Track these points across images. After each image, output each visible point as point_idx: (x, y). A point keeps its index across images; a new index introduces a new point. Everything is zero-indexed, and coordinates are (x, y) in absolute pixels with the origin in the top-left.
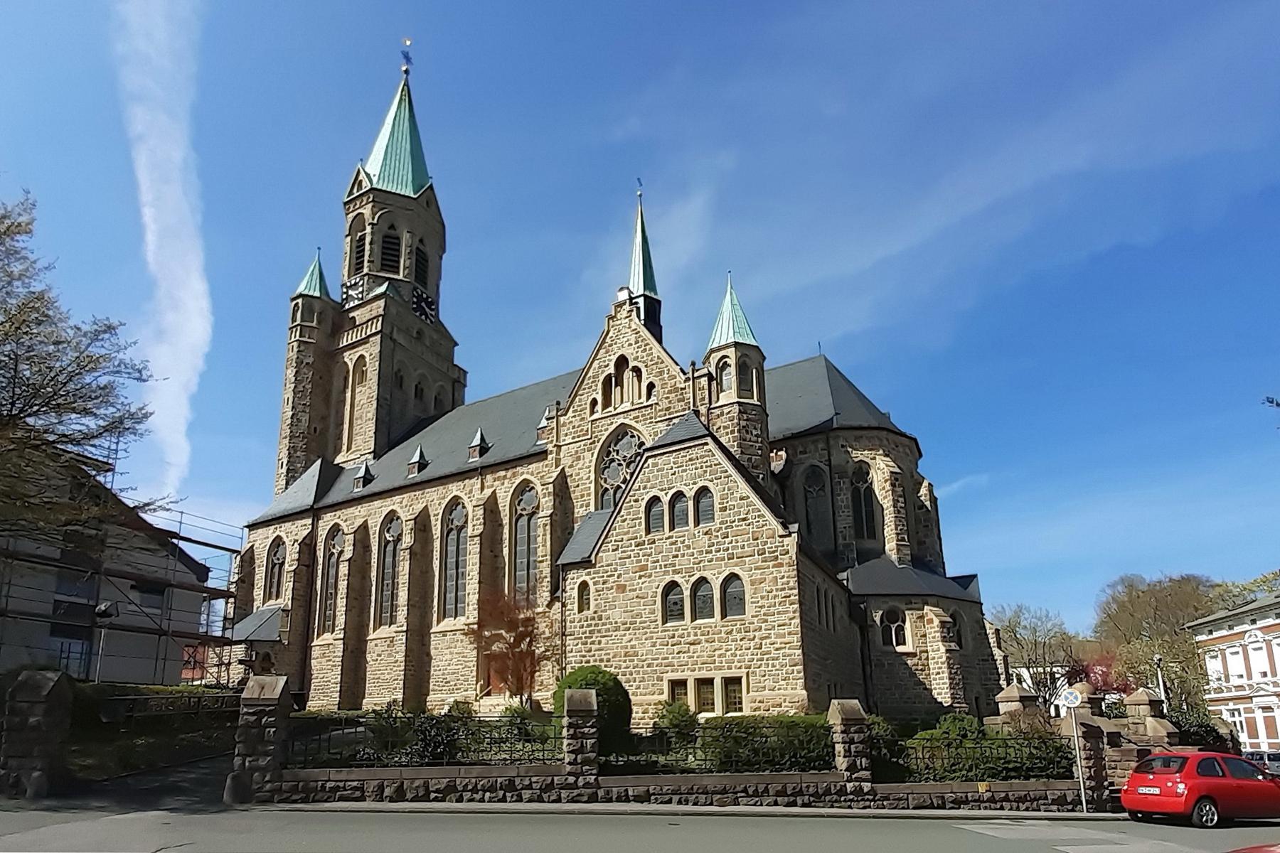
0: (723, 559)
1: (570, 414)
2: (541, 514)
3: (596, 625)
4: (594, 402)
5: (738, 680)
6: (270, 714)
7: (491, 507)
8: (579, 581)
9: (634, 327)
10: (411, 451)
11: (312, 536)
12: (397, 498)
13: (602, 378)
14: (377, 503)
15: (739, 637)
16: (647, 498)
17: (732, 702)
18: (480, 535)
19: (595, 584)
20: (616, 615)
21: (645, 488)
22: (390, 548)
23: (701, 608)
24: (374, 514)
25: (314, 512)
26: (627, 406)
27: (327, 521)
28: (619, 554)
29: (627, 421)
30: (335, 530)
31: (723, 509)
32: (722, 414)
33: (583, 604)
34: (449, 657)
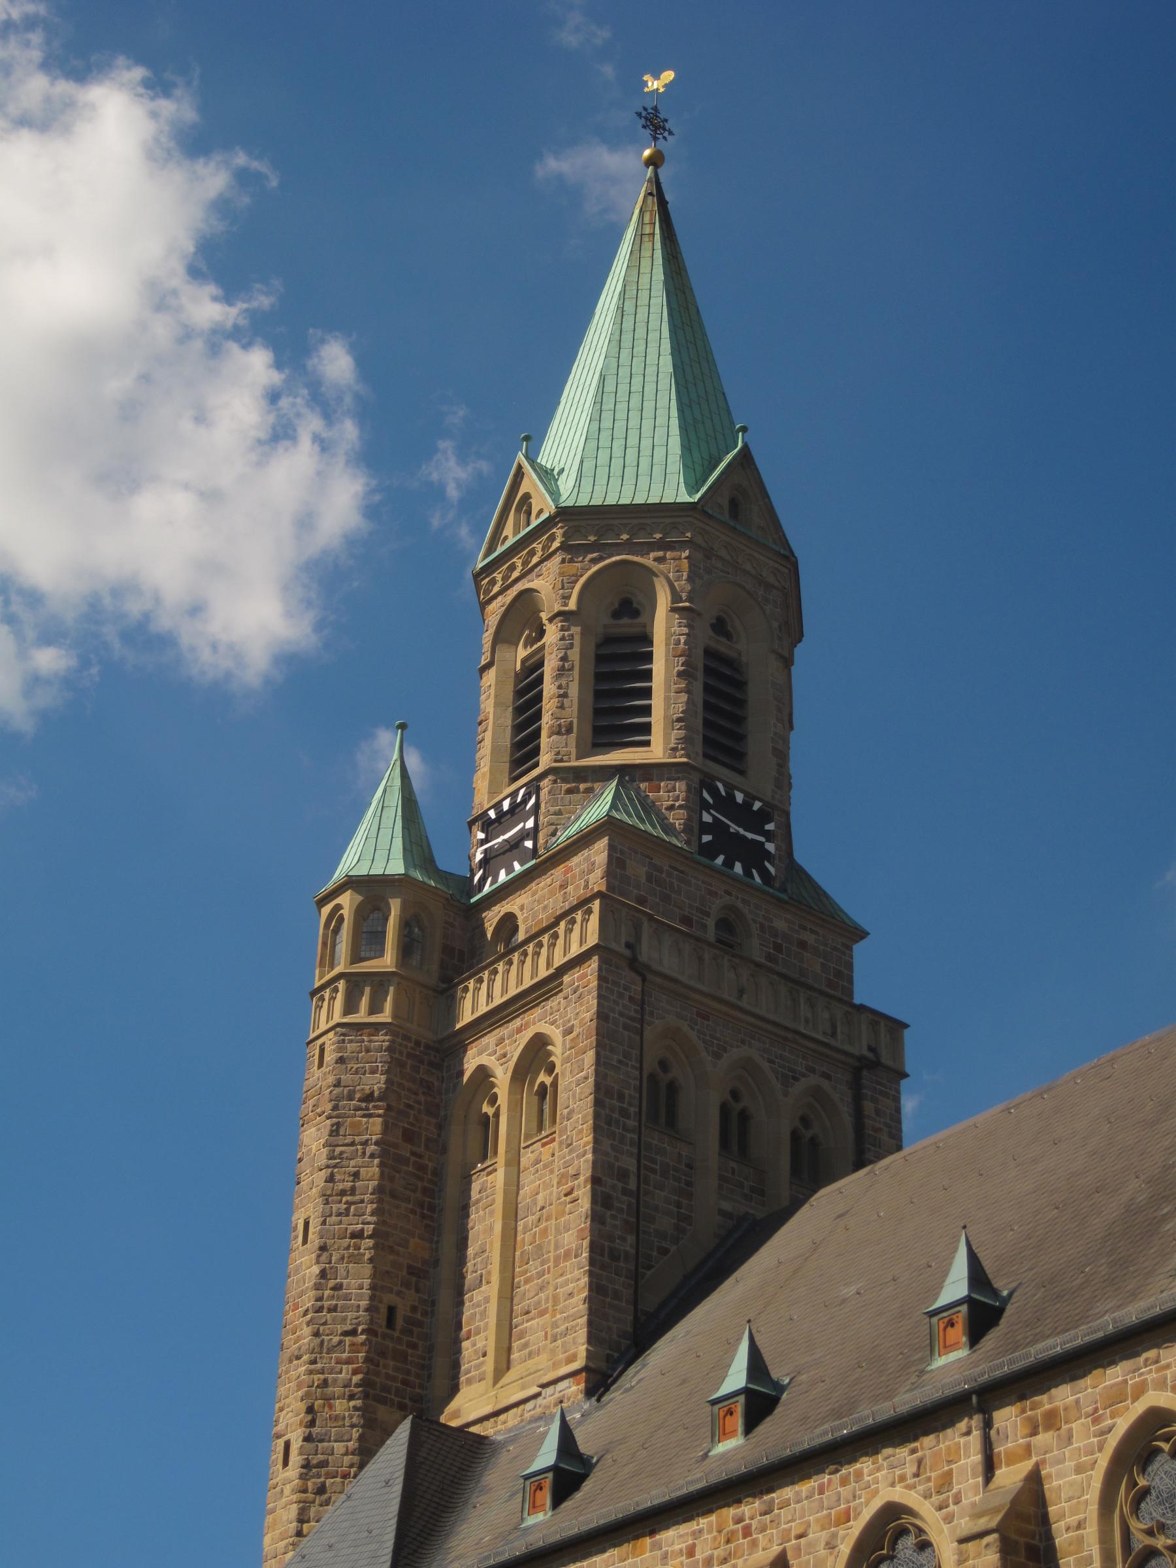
10: (709, 1348)
33: (546, 1333)
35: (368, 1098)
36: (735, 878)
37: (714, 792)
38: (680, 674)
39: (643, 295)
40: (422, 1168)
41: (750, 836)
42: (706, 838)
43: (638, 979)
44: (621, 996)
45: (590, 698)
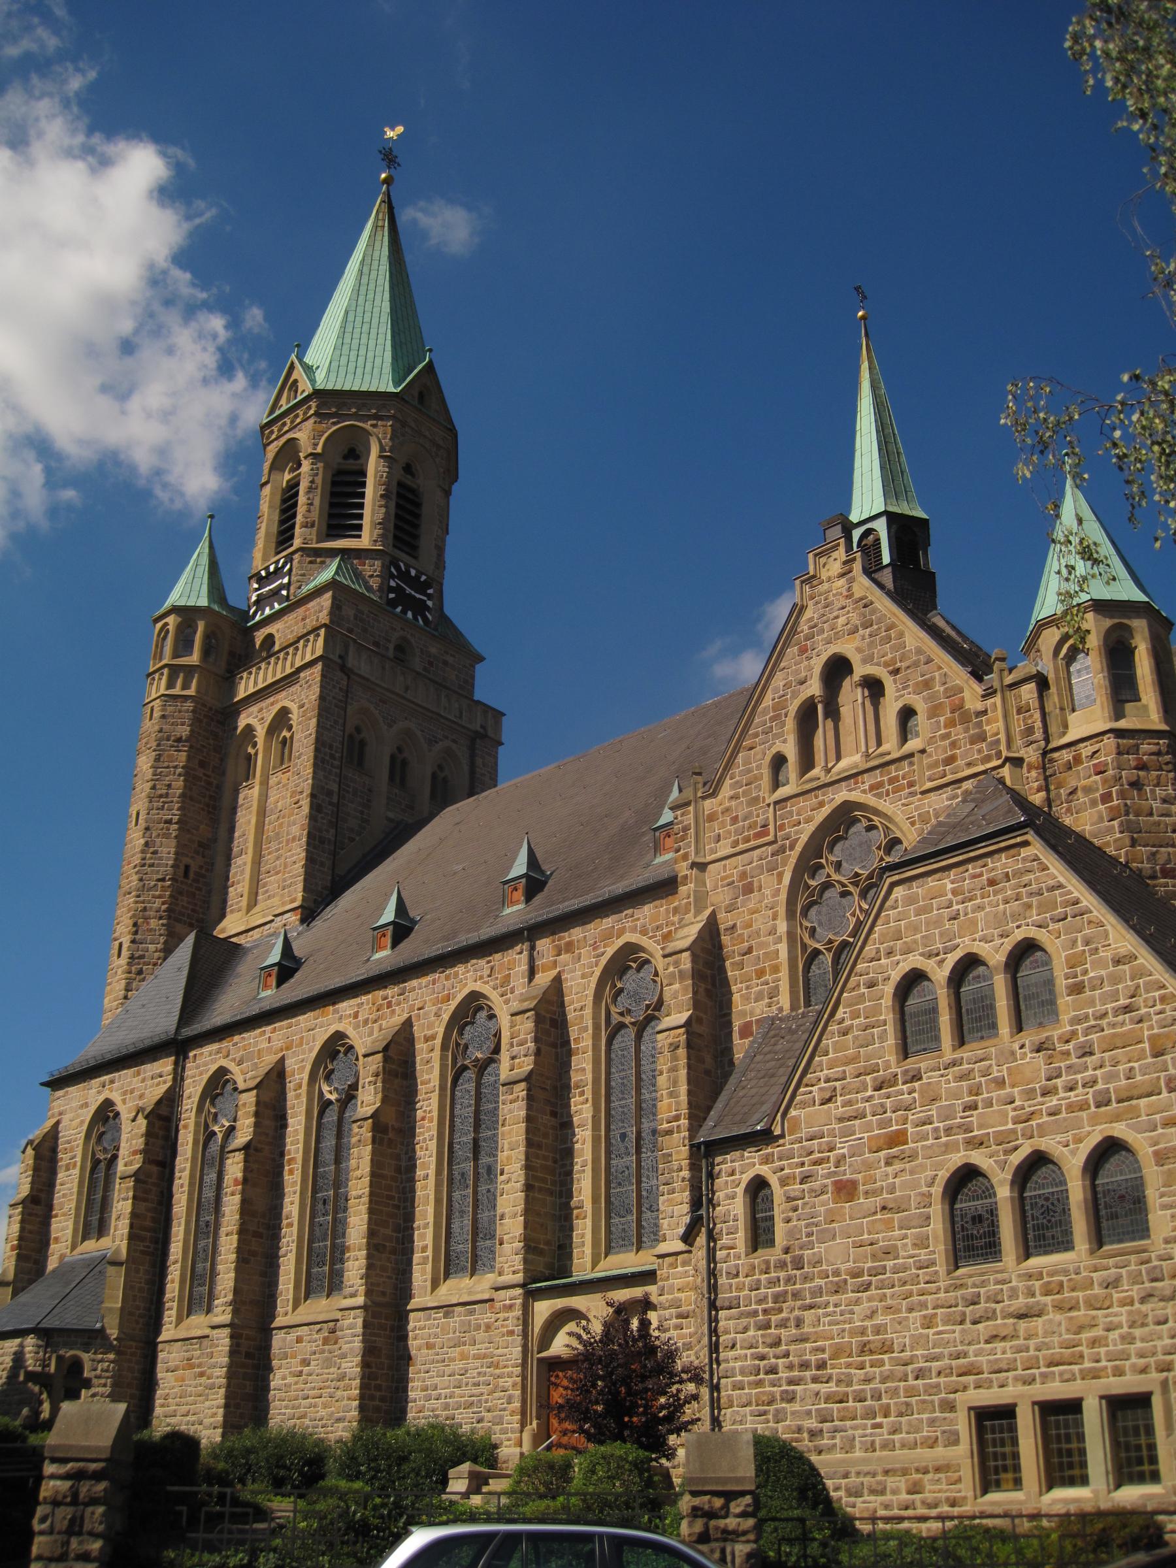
0: (1083, 1106)
1: (726, 791)
2: (667, 1022)
3: (789, 1280)
4: (779, 761)
5: (1142, 1401)
6: (97, 1476)
7: (550, 1017)
8: (746, 1178)
9: (858, 592)
10: (374, 898)
11: (169, 1103)
12: (346, 1007)
13: (794, 707)
14: (304, 1020)
15: (1135, 1292)
16: (896, 975)
17: (1135, 1461)
18: (528, 1078)
19: (784, 1182)
20: (836, 1254)
21: (890, 953)
22: (331, 1116)
23: (1043, 1230)
24: (299, 1042)
25: (178, 1047)
26: (851, 760)
27: (204, 1062)
28: (837, 1108)
29: (855, 796)
30: (219, 1083)
31: (1077, 989)
32: (1077, 760)
33: (760, 1233)
34: (458, 1365)
35: (179, 740)
36: (407, 620)
37: (398, 568)
38: (382, 496)
39: (375, 263)
40: (209, 783)
41: (418, 596)
42: (392, 596)
43: (345, 678)
44: (334, 687)
45: (326, 506)
